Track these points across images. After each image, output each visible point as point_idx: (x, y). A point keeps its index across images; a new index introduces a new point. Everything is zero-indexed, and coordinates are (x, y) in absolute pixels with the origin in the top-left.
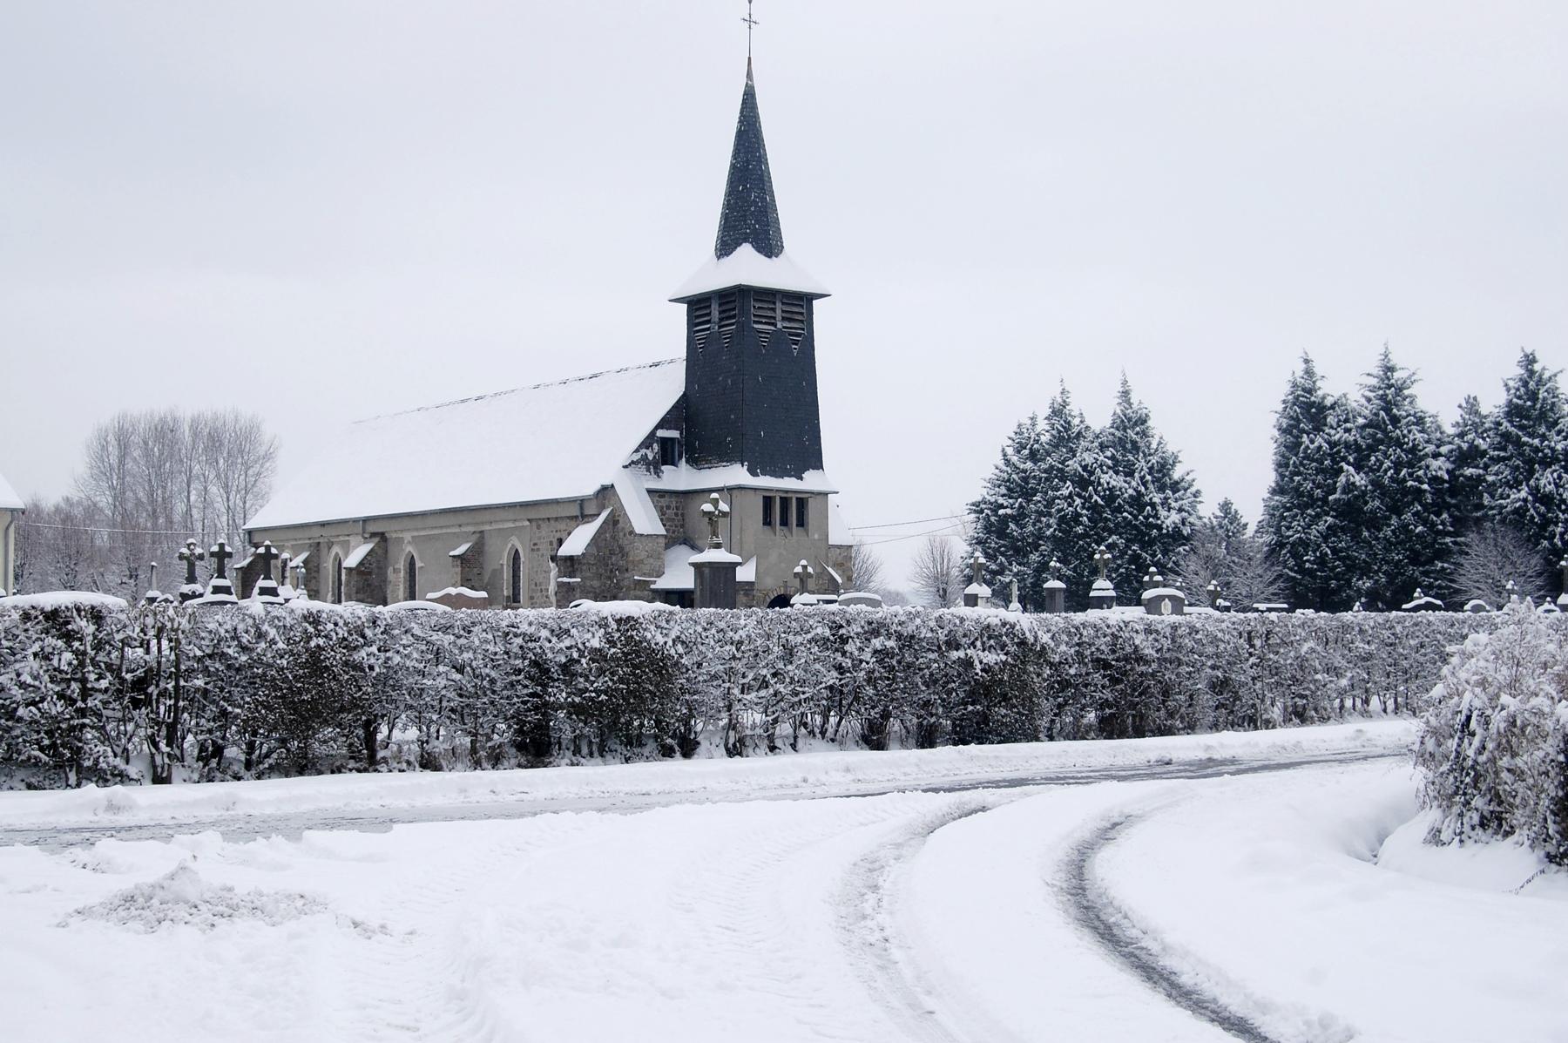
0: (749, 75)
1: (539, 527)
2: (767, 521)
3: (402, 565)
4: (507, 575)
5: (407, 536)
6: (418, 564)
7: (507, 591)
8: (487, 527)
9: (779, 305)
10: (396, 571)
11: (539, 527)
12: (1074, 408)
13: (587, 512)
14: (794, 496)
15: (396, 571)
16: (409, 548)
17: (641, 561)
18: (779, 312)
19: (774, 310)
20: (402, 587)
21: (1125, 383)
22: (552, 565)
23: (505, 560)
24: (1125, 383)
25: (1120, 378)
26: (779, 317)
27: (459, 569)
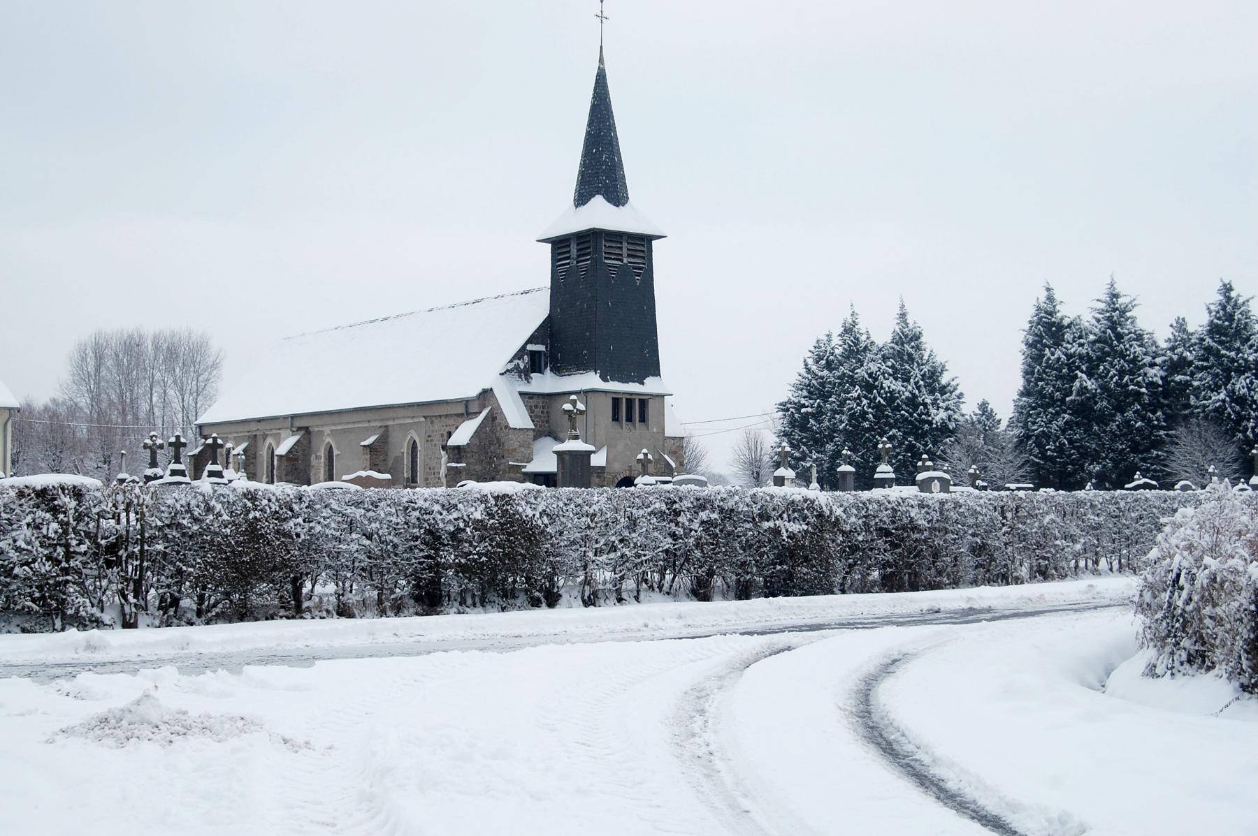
0: (601, 60)
1: (432, 423)
3: (322, 453)
4: (406, 461)
5: (327, 430)
6: (336, 452)
9: (625, 245)
10: (318, 458)
11: (432, 423)
12: (862, 327)
14: (637, 398)
15: (318, 458)
16: (328, 440)
17: (515, 450)
18: (625, 250)
19: (621, 248)
20: (322, 471)
21: (903, 306)
22: (443, 453)
23: (405, 449)
24: (903, 306)
27: (368, 456)
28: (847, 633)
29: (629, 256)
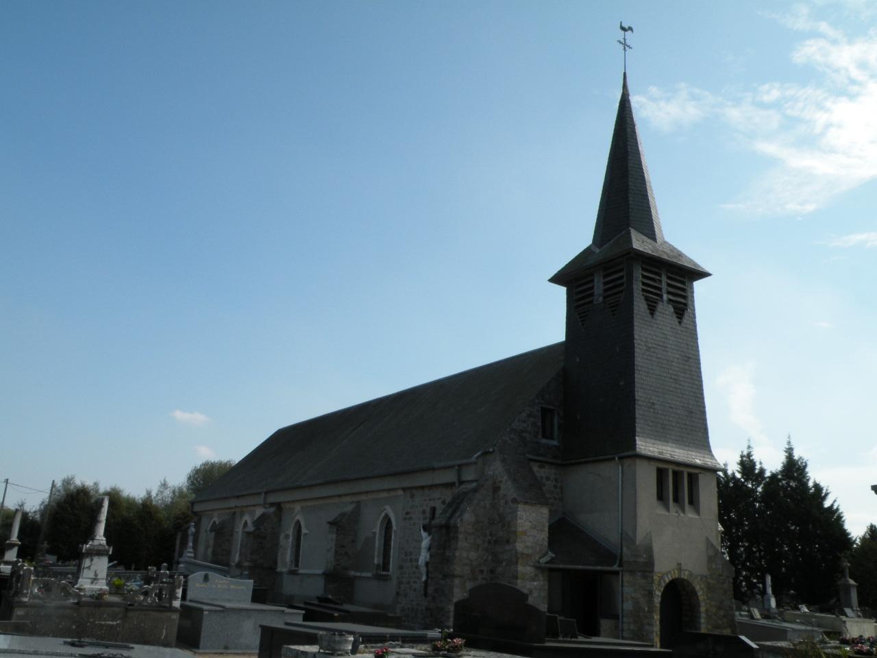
0: (625, 86)
1: (412, 496)
2: (661, 496)
3: (291, 531)
4: (378, 543)
5: (297, 507)
6: (304, 531)
7: (683, 306)
8: (363, 497)
9: (664, 279)
10: (287, 537)
11: (412, 496)
12: (756, 457)
13: (464, 478)
14: (671, 468)
15: (287, 537)
16: (299, 517)
17: (525, 533)
18: (664, 286)
19: (660, 281)
20: (289, 551)
21: (789, 443)
22: (424, 534)
23: (377, 529)
24: (789, 443)
25: (786, 440)
26: (664, 286)
27: (334, 536)
28: (3, 494)
29: (669, 293)
